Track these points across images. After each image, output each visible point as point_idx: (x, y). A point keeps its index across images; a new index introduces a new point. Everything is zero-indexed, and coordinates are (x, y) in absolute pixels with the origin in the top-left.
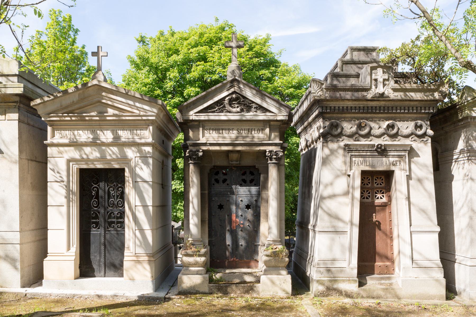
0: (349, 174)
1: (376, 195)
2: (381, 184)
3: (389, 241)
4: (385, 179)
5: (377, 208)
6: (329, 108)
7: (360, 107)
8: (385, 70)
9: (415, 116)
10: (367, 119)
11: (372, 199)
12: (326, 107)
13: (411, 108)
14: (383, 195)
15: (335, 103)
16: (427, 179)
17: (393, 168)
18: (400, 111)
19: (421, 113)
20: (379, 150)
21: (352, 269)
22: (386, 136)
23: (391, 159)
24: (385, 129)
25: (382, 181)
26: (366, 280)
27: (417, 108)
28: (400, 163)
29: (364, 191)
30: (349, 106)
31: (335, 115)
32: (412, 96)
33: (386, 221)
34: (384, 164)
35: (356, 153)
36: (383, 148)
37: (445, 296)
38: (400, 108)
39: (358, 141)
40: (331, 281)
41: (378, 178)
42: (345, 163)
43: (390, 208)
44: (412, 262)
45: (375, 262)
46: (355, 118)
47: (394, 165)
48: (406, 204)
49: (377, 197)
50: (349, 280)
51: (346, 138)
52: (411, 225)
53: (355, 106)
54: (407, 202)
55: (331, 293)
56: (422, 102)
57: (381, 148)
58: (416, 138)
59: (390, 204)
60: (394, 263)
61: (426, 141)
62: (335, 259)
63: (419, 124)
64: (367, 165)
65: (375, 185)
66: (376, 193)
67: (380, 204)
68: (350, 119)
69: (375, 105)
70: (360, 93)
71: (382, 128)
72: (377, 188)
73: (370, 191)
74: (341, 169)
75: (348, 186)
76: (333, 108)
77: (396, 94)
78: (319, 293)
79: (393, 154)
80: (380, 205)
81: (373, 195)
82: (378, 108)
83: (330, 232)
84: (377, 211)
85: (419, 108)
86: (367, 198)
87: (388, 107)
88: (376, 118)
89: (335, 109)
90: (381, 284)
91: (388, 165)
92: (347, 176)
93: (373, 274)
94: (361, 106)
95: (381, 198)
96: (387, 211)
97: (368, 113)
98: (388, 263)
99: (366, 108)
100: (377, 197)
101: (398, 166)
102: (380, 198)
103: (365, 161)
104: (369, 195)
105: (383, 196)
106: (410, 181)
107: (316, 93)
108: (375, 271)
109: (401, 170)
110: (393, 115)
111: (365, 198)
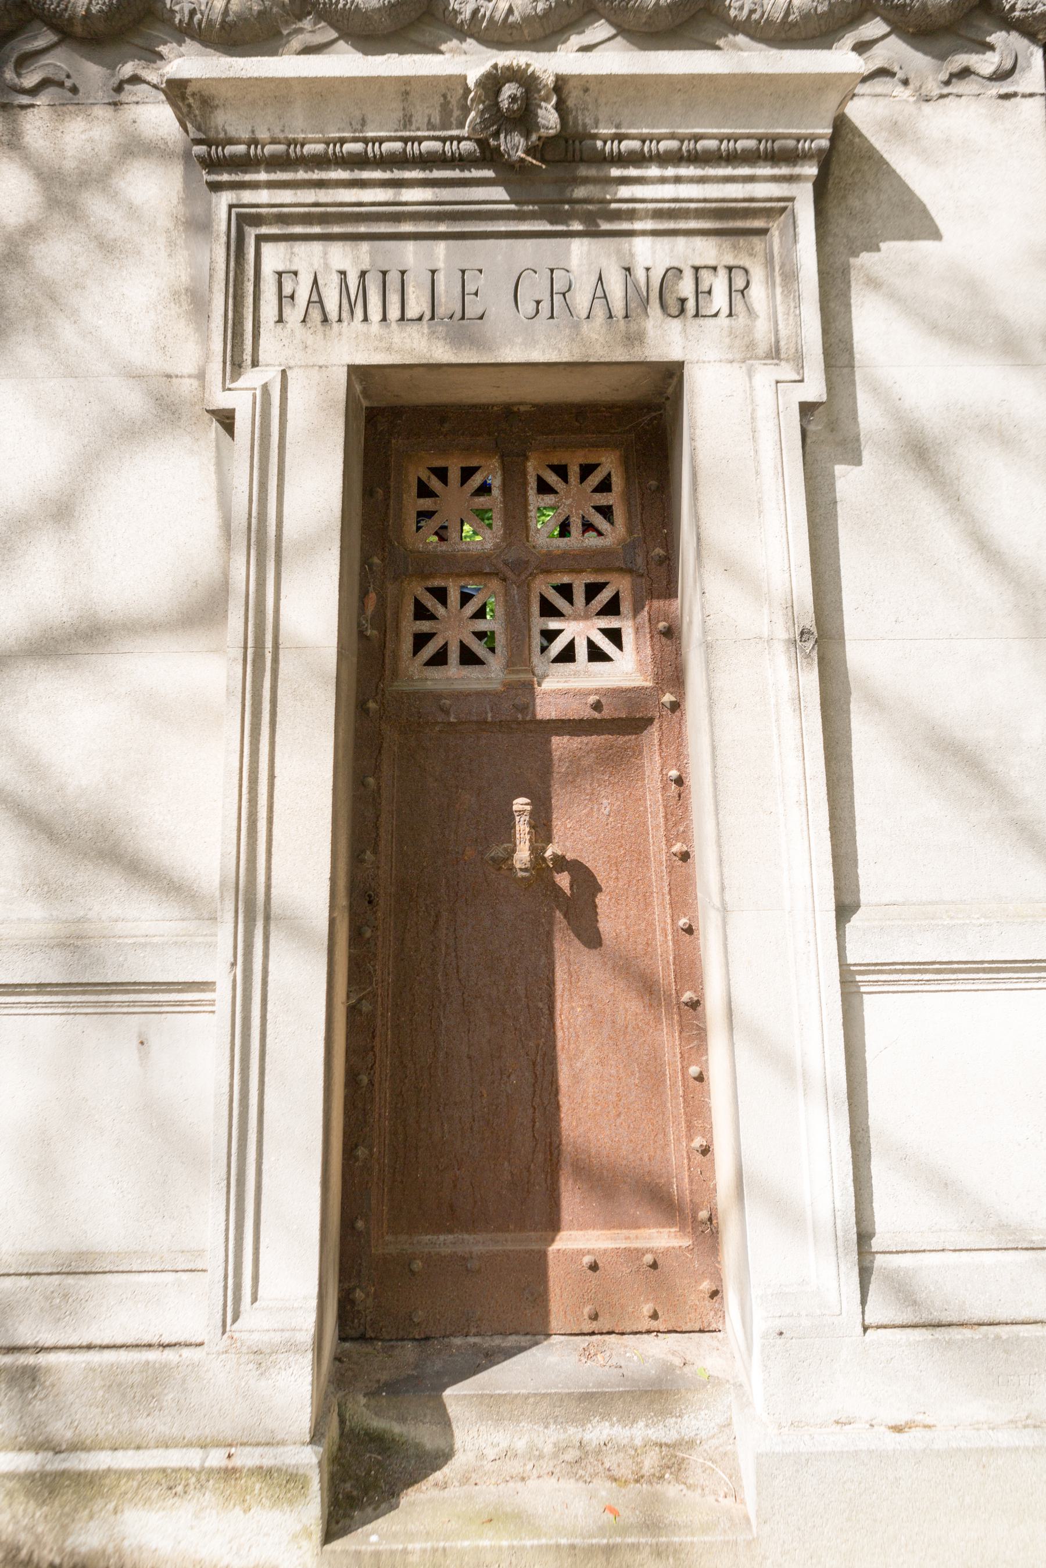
0: (222, 400)
1: (553, 624)
5: (559, 744)
11: (510, 665)
25: (602, 499)
26: (445, 1423)
28: (738, 293)
29: (441, 595)
33: (642, 857)
34: (581, 299)
35: (286, 196)
36: (548, 117)
41: (562, 471)
44: (865, 1273)
45: (553, 1225)
48: (798, 698)
49: (558, 646)
50: (229, 1473)
52: (845, 910)
54: (811, 679)
59: (675, 706)
61: (1001, 75)
62: (82, 1255)
64: (412, 312)
66: (549, 610)
67: (584, 711)
72: (549, 563)
74: (156, 363)
80: (588, 713)
83: (41, 988)
84: (560, 769)
86: (468, 658)
91: (618, 307)
95: (596, 654)
100: (558, 646)
101: (723, 320)
102: (582, 651)
105: (615, 636)
106: (839, 469)
111: (454, 654)
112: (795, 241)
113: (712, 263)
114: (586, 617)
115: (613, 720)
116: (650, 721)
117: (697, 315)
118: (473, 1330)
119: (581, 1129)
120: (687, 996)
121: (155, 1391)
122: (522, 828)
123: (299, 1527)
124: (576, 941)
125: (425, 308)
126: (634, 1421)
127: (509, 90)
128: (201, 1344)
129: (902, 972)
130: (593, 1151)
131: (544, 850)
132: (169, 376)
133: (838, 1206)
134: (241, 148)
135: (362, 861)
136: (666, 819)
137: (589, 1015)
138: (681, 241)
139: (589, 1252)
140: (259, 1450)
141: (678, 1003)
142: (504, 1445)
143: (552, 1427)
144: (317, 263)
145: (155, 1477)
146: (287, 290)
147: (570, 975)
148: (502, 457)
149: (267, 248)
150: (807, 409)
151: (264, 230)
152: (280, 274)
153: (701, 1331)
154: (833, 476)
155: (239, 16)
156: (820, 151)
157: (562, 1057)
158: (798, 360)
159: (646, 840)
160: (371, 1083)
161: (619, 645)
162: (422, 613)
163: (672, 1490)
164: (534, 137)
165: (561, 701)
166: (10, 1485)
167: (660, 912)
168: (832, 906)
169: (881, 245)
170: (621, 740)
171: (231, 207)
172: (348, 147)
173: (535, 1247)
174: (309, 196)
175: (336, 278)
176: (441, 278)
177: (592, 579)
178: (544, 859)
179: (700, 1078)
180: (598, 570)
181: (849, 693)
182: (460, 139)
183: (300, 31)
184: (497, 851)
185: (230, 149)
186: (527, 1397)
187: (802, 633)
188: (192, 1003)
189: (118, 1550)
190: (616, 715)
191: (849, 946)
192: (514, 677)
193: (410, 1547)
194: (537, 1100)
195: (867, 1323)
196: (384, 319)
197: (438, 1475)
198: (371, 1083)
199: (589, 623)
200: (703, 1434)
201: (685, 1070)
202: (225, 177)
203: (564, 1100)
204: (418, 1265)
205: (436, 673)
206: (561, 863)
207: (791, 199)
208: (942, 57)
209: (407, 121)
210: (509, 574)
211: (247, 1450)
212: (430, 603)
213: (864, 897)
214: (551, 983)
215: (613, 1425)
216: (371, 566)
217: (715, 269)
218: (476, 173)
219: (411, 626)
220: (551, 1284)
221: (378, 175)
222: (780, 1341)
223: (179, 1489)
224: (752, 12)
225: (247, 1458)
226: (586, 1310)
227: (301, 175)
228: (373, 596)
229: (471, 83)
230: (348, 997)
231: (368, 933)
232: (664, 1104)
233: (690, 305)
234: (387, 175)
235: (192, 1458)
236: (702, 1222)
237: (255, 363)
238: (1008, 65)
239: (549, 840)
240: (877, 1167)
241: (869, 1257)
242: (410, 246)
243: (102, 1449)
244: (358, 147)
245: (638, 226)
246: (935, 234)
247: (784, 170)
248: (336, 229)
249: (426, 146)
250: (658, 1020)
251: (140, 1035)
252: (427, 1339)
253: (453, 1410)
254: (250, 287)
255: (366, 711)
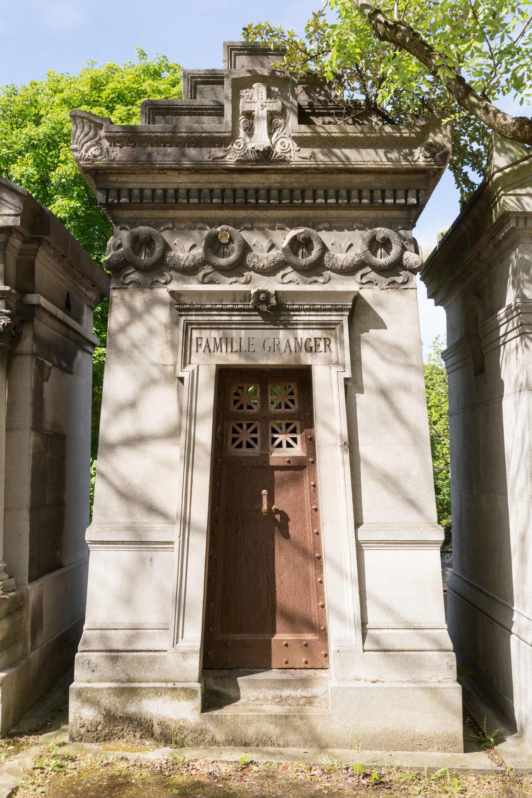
0: (180, 374)
1: (275, 436)
2: (287, 407)
3: (311, 569)
4: (299, 392)
5: (277, 473)
6: (125, 193)
7: (211, 191)
8: (276, 89)
9: (372, 214)
10: (237, 224)
11: (262, 448)
12: (119, 191)
13: (354, 193)
14: (294, 436)
15: (141, 178)
16: (406, 388)
17: (307, 359)
18: (323, 201)
19: (384, 207)
20: (264, 308)
21: (184, 654)
22: (289, 269)
23: (303, 335)
24: (284, 250)
26: (238, 688)
27: (372, 192)
28: (327, 346)
29: (241, 426)
30: (182, 186)
31: (146, 213)
32: (347, 158)
33: (303, 510)
35: (200, 318)
36: (273, 301)
37: (461, 738)
38: (326, 192)
39: (212, 282)
40: (120, 692)
42: (173, 346)
43: (314, 474)
44: (364, 636)
45: (273, 632)
46: (202, 220)
47: (310, 350)
49: (277, 442)
50: (174, 689)
51: (178, 275)
52: (358, 524)
53: (198, 186)
54: (347, 457)
55: (120, 728)
56: (384, 177)
57: (267, 301)
58: (373, 275)
59: (314, 462)
60: (326, 634)
61: (404, 283)
63: (379, 237)
64: (234, 350)
65: (272, 408)
66: (274, 431)
68: (189, 224)
69: (256, 185)
70: (205, 150)
71: (278, 249)
72: (275, 417)
73: (257, 424)
74: (161, 362)
75: (181, 411)
76: (136, 192)
77: (306, 152)
78: (83, 730)
79: (307, 318)
80: (286, 464)
81: (265, 437)
82: (263, 192)
83: (123, 542)
84: (277, 481)
85: (379, 192)
86: (249, 446)
87: (292, 191)
88: (263, 220)
89: (142, 197)
90: (281, 701)
91: (293, 349)
92: (177, 381)
93: (267, 667)
94: (216, 186)
95: (289, 445)
96: (307, 482)
97: (234, 206)
98: (309, 637)
99: (229, 193)
100: (277, 442)
101: (323, 353)
102: (284, 444)
103: (228, 341)
104: (254, 436)
105: (295, 440)
106: (357, 395)
107: (83, 151)
108: (273, 659)
109: (330, 363)
110: (310, 213)
111: (244, 444)
112: (343, 332)
113: (320, 337)
114: (286, 433)
115: (294, 466)
116: (305, 467)
117: (315, 352)
118: (247, 666)
119: (283, 599)
120: (317, 555)
121: (152, 664)
122: (265, 499)
123: (194, 707)
124: (282, 537)
125: (238, 348)
126: (297, 689)
127: (262, 296)
128: (166, 651)
129: (375, 543)
130: (287, 607)
131: (272, 507)
132: (164, 365)
133: (355, 612)
134: (188, 306)
135: (215, 509)
136: (310, 498)
137: (286, 561)
138: (311, 331)
139: (285, 640)
140: (183, 683)
141: (314, 557)
142: (256, 696)
143: (271, 691)
144: (208, 335)
145: (152, 690)
146: (199, 343)
147: (280, 548)
148: (260, 384)
149: (194, 332)
150: (346, 380)
151: (193, 326)
152: (197, 338)
153: (322, 669)
154: (355, 397)
155: (187, 266)
156: (349, 309)
157: (277, 575)
158: (344, 366)
159: (304, 505)
160: (216, 582)
161: (296, 443)
162: (235, 431)
163: (308, 707)
164: (269, 306)
165: (278, 460)
166: (109, 691)
167: (309, 528)
168: (353, 523)
169: (370, 331)
170: (297, 472)
171: (184, 321)
172: (218, 306)
173: (268, 638)
174: (206, 318)
175: (213, 340)
176: (243, 340)
177: (288, 422)
178: (272, 510)
179: (321, 582)
180: (290, 419)
181: (360, 461)
182: (249, 305)
183: (204, 269)
184: (257, 507)
185: (185, 306)
186: (264, 680)
187: (344, 443)
188: (166, 548)
189: (140, 713)
190: (295, 465)
191: (359, 535)
192: (263, 452)
193: (227, 714)
194: (269, 589)
195: (365, 649)
196: (227, 351)
197: (235, 704)
198: (216, 582)
199: (287, 435)
200: (319, 694)
201: (316, 579)
202: (183, 313)
203: (277, 589)
204: (229, 643)
205: (239, 450)
206: (277, 511)
207: (342, 321)
208: (387, 277)
209: (234, 300)
210: (262, 420)
211: (179, 683)
212: (237, 428)
213: (364, 521)
214: (274, 550)
215: (290, 690)
216: (219, 417)
217: (320, 339)
218: (253, 313)
219: (231, 435)
220: (273, 651)
221: (226, 313)
222: (338, 654)
223: (159, 694)
224: (332, 266)
225: (179, 685)
226: (284, 660)
227: (204, 313)
228: (220, 426)
229: (252, 293)
230: (209, 553)
231: (216, 532)
232: (310, 591)
233: (314, 349)
234: (228, 313)
235: (164, 685)
236: (322, 631)
237: (190, 363)
238: (406, 280)
239: (273, 504)
240: (369, 603)
241: (366, 630)
242: (234, 331)
243: (136, 682)
244: (221, 306)
245: (299, 327)
246: (385, 328)
247: (339, 313)
248: (214, 327)
249: (239, 306)
250: (308, 563)
251: (151, 557)
252: (232, 669)
253: (240, 684)
254: (189, 342)
255: (217, 462)
